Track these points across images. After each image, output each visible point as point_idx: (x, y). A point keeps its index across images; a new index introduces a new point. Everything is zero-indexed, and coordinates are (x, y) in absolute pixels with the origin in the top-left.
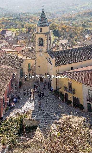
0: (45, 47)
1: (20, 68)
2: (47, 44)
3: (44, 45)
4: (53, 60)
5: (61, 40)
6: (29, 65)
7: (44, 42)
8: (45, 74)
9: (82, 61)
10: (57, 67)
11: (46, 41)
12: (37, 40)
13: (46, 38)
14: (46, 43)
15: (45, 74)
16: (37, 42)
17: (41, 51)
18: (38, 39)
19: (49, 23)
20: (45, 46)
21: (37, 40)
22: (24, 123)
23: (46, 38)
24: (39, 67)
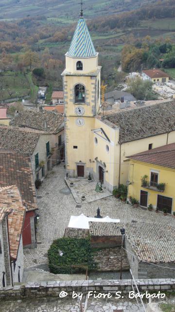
0: (88, 104)
1: (35, 153)
2: (93, 99)
3: (87, 101)
4: (114, 133)
5: (55, 92)
6: (48, 144)
7: (89, 94)
8: (90, 160)
9: (169, 132)
10: (124, 146)
11: (93, 92)
12: (70, 90)
13: (92, 84)
14: (93, 97)
15: (90, 160)
16: (69, 95)
17: (79, 116)
18: (72, 88)
19: (40, 59)
20: (89, 103)
21: (70, 90)
22: (118, 269)
23: (92, 84)
24: (75, 147)
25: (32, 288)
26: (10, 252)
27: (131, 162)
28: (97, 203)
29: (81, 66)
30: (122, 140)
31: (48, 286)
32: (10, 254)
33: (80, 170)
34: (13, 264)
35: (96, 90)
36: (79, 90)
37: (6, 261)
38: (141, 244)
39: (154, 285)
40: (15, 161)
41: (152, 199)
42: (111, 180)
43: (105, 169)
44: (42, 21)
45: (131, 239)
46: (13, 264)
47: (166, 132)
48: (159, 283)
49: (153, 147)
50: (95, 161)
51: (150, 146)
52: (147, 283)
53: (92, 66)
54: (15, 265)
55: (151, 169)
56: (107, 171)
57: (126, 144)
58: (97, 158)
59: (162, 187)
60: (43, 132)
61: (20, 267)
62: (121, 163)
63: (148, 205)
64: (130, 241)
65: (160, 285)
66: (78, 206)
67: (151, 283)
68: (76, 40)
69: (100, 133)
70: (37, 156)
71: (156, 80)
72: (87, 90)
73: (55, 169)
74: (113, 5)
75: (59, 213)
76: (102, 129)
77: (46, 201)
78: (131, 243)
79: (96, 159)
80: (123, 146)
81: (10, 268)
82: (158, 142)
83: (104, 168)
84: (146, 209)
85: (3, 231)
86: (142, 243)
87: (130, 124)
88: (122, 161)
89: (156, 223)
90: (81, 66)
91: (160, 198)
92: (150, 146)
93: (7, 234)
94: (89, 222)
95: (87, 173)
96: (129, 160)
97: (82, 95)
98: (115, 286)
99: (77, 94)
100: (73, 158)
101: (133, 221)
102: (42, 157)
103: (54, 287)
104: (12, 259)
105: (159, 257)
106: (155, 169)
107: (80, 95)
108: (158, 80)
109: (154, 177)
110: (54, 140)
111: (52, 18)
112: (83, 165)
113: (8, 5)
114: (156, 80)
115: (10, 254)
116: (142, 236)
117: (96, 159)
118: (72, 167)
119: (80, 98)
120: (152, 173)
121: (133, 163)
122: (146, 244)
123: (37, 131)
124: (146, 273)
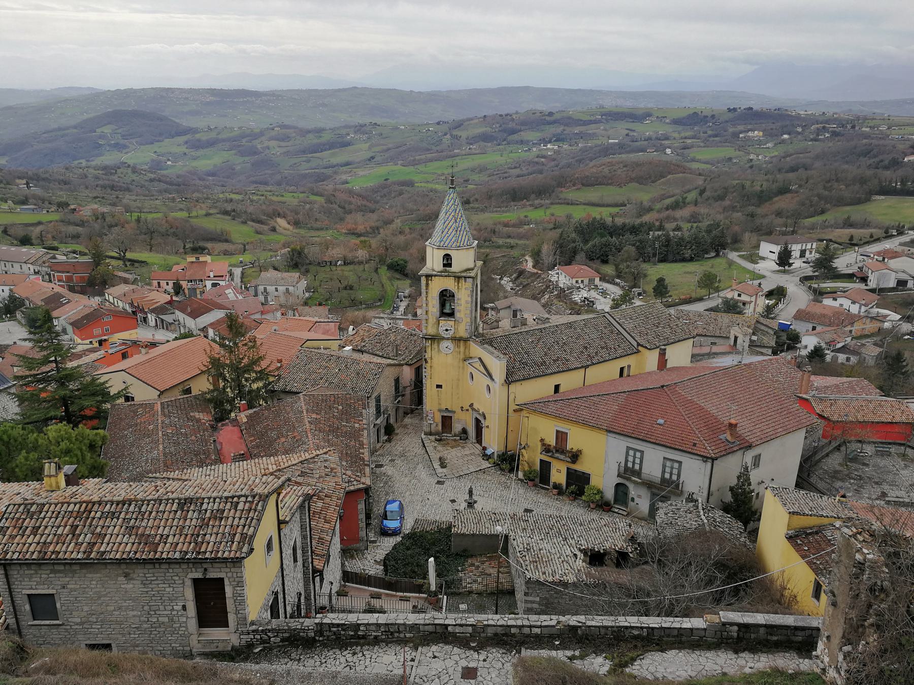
1: (375, 394)
6: (397, 381)
9: (588, 366)
24: (439, 386)
25: (333, 625)
26: (312, 559)
27: (524, 413)
28: (470, 477)
29: (449, 262)
30: (510, 379)
31: (358, 622)
32: (312, 562)
33: (447, 421)
34: (318, 579)
35: (472, 299)
36: (446, 297)
37: (305, 574)
38: (532, 550)
39: (530, 627)
40: (340, 407)
41: (558, 475)
42: (494, 443)
43: (484, 423)
44: (407, 188)
45: (518, 542)
46: (318, 579)
47: (582, 367)
48: (539, 623)
49: (561, 390)
50: (470, 409)
51: (557, 388)
52: (519, 623)
53: (464, 260)
54: (322, 580)
55: (556, 426)
56: (488, 427)
57: (518, 384)
58: (472, 404)
59: (575, 456)
60: (389, 361)
61: (332, 583)
62: (510, 415)
63: (551, 484)
64: (515, 543)
65: (541, 627)
66: (439, 482)
67: (526, 623)
68: (443, 221)
69: (478, 365)
70: (378, 400)
71: (580, 282)
72: (458, 299)
73: (407, 420)
74: (518, 165)
75: (408, 493)
76: (480, 359)
77: (390, 473)
78: (517, 547)
79: (471, 405)
80: (512, 387)
81: (312, 586)
82: (570, 381)
83: (483, 421)
84: (548, 489)
85: (302, 526)
86: (535, 548)
87: (526, 353)
88: (511, 411)
89: (562, 514)
90: (449, 262)
91: (571, 474)
92: (557, 388)
93: (308, 529)
94: (580, 452)
95: (457, 428)
96: (522, 410)
97: (451, 305)
98: (467, 625)
99: (442, 305)
100: (432, 401)
101: (526, 511)
102: (387, 403)
103: (368, 624)
104: (315, 571)
105: (560, 572)
106: (563, 427)
107: (447, 305)
108: (582, 282)
109: (561, 436)
110: (408, 374)
111: (423, 185)
112: (450, 415)
113: (359, 163)
114: (580, 282)
115: (312, 562)
116: (536, 538)
117: (471, 405)
118: (433, 419)
119: (447, 311)
120: (557, 432)
121: (528, 415)
122: (540, 550)
123: (379, 360)
124: (538, 599)
